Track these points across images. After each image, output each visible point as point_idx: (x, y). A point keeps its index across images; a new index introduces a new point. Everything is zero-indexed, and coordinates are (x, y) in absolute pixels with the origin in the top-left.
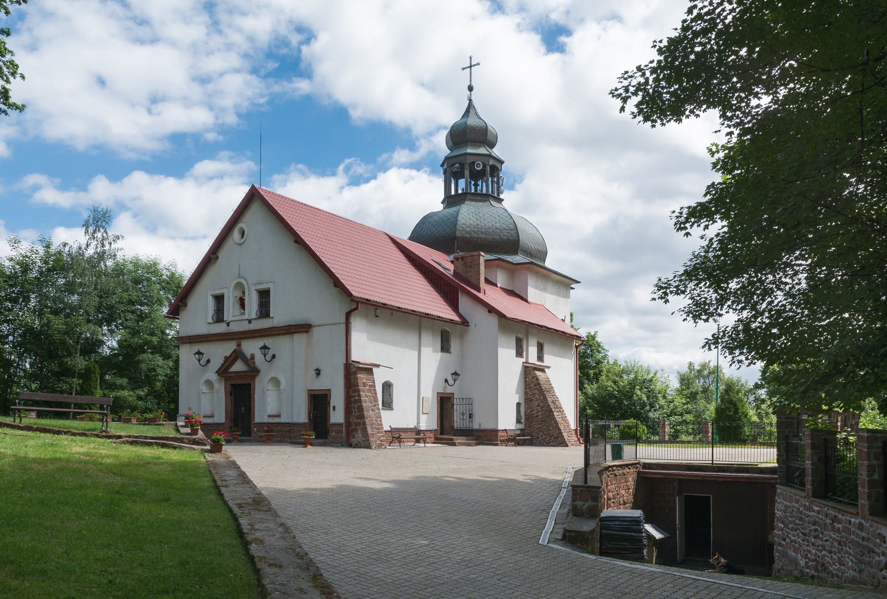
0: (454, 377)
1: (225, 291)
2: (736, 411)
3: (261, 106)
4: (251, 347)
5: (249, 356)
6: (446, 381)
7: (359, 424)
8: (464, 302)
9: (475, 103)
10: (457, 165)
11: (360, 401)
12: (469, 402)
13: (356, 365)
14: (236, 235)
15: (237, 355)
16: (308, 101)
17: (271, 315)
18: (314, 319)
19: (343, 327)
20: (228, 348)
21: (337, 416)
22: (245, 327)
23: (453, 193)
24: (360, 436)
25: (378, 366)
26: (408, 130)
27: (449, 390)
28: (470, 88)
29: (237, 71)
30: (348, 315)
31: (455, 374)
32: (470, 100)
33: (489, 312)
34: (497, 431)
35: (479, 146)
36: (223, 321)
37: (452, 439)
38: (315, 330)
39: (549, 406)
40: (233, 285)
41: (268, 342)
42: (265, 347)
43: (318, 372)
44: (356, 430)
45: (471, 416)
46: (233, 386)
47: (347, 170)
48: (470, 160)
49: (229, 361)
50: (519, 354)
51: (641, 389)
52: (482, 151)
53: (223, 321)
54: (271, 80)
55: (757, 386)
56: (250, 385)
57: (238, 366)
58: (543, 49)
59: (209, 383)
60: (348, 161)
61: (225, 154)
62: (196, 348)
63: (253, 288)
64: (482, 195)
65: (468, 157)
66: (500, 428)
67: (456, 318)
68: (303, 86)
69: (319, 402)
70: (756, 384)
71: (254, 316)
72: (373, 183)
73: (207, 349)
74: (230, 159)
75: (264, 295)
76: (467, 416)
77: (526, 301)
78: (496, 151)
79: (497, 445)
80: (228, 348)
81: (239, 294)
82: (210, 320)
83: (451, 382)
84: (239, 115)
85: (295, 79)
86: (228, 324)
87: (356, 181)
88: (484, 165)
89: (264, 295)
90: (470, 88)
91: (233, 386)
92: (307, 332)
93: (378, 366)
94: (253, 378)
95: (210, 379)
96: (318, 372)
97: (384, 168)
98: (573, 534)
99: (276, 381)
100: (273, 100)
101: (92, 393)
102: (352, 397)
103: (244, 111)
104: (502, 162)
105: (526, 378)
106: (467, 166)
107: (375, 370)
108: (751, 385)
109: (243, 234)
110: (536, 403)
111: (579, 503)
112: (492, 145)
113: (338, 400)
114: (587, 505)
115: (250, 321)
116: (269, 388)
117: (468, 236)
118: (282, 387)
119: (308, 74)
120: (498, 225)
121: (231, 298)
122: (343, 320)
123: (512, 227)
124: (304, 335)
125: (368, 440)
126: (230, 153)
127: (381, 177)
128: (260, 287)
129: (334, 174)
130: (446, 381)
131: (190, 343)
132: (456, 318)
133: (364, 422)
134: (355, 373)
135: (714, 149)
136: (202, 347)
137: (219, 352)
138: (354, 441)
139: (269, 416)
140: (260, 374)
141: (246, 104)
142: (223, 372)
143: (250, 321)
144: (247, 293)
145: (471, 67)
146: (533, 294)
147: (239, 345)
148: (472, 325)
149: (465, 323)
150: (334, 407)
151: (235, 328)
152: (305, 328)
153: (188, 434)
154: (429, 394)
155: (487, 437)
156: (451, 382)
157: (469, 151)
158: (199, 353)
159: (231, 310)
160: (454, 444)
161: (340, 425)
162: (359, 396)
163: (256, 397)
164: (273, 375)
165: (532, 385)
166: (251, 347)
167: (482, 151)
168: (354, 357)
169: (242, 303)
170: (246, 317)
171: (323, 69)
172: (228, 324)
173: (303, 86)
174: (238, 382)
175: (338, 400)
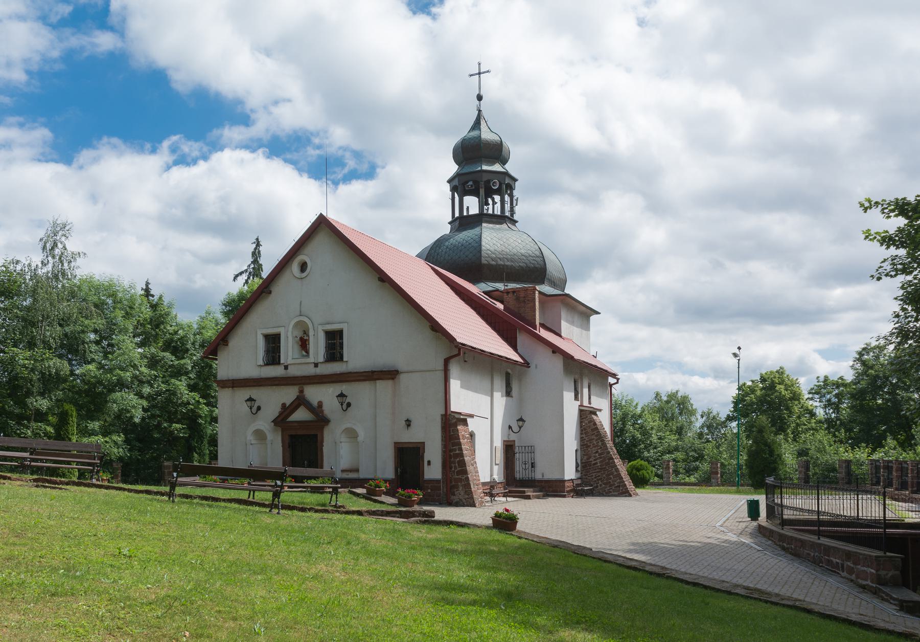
0: (520, 423)
1: (282, 331)
2: (772, 452)
3: (55, 61)
4: (314, 394)
5: (315, 404)
6: (510, 427)
7: (461, 480)
8: (521, 339)
9: (484, 113)
10: (471, 183)
11: (462, 455)
12: (531, 450)
13: (457, 416)
14: (295, 267)
15: (301, 401)
16: (118, 60)
17: (345, 359)
18: (401, 365)
19: (441, 375)
20: (288, 395)
21: (433, 471)
22: (311, 371)
23: (465, 214)
24: (462, 493)
25: (472, 416)
26: (239, 102)
27: (513, 437)
28: (480, 98)
29: (21, 18)
30: (447, 362)
31: (521, 420)
32: (480, 111)
33: (554, 352)
34: (564, 481)
35: (493, 164)
36: (279, 363)
37: (524, 492)
38: (402, 377)
39: (609, 452)
40: (293, 323)
41: (344, 388)
42: (342, 395)
43: (408, 423)
44: (456, 487)
45: (533, 465)
46: (292, 437)
47: (173, 150)
48: (485, 177)
49: (287, 410)
50: (576, 398)
51: (633, 425)
52: (497, 167)
53: (279, 363)
54: (67, 31)
55: (730, 418)
56: (316, 436)
57: (301, 415)
58: (410, 14)
59: (260, 435)
60: (175, 138)
61: (13, 119)
62: (245, 393)
63: (320, 328)
64: (488, 215)
65: (484, 174)
66: (566, 478)
67: (517, 358)
68: (105, 41)
69: (409, 457)
70: (728, 416)
71: (321, 359)
72: (202, 166)
73: (261, 395)
74: (21, 125)
75: (335, 339)
76: (529, 466)
77: (560, 336)
78: (510, 167)
79: (564, 496)
80: (288, 395)
81: (299, 334)
82: (261, 363)
83: (516, 429)
84: (28, 72)
85: (97, 33)
86: (286, 368)
87: (183, 160)
88: (501, 184)
89: (335, 339)
90: (480, 98)
91: (292, 437)
92: (393, 379)
93: (472, 416)
94: (321, 429)
95: (262, 428)
96: (408, 423)
97: (217, 146)
98: (911, 604)
99: (352, 434)
100: (69, 56)
101: (70, 440)
102: (451, 451)
103: (35, 68)
104: (515, 180)
105: (581, 422)
106: (482, 184)
107: (469, 420)
108: (723, 417)
109: (303, 267)
110: (594, 450)
111: (882, 573)
112: (504, 162)
113: (433, 455)
114: (890, 574)
115: (316, 365)
116: (343, 439)
117: (493, 263)
118: (360, 439)
119: (119, 30)
120: (523, 251)
121: (290, 339)
122: (441, 366)
123: (538, 253)
124: (390, 382)
125: (472, 498)
126: (21, 119)
127: (216, 157)
128: (330, 327)
129: (154, 151)
130: (510, 427)
131: (233, 387)
132: (517, 358)
133: (467, 479)
134: (456, 425)
135: (867, 204)
136: (254, 392)
137: (274, 400)
138: (455, 499)
139: (343, 471)
140: (331, 425)
141: (37, 58)
142: (281, 421)
143: (316, 365)
144: (311, 333)
145: (479, 74)
146: (566, 327)
147: (301, 391)
148: (532, 366)
149: (527, 364)
150: (429, 463)
151: (294, 371)
152: (391, 374)
153: (392, 505)
154: (498, 443)
155: (552, 488)
156: (516, 429)
157: (485, 167)
158: (251, 399)
159: (289, 351)
160: (528, 497)
161: (438, 481)
162: (461, 449)
163: (325, 449)
164: (349, 425)
165: (589, 430)
166: (314, 394)
167: (497, 167)
168: (454, 407)
169: (304, 344)
170: (311, 359)
171: (137, 26)
172: (286, 368)
173: (105, 41)
174: (300, 432)
175: (433, 455)
